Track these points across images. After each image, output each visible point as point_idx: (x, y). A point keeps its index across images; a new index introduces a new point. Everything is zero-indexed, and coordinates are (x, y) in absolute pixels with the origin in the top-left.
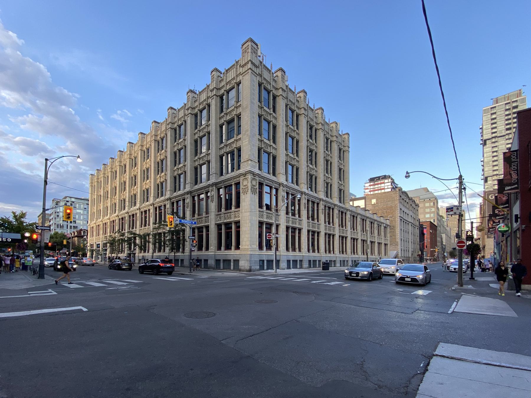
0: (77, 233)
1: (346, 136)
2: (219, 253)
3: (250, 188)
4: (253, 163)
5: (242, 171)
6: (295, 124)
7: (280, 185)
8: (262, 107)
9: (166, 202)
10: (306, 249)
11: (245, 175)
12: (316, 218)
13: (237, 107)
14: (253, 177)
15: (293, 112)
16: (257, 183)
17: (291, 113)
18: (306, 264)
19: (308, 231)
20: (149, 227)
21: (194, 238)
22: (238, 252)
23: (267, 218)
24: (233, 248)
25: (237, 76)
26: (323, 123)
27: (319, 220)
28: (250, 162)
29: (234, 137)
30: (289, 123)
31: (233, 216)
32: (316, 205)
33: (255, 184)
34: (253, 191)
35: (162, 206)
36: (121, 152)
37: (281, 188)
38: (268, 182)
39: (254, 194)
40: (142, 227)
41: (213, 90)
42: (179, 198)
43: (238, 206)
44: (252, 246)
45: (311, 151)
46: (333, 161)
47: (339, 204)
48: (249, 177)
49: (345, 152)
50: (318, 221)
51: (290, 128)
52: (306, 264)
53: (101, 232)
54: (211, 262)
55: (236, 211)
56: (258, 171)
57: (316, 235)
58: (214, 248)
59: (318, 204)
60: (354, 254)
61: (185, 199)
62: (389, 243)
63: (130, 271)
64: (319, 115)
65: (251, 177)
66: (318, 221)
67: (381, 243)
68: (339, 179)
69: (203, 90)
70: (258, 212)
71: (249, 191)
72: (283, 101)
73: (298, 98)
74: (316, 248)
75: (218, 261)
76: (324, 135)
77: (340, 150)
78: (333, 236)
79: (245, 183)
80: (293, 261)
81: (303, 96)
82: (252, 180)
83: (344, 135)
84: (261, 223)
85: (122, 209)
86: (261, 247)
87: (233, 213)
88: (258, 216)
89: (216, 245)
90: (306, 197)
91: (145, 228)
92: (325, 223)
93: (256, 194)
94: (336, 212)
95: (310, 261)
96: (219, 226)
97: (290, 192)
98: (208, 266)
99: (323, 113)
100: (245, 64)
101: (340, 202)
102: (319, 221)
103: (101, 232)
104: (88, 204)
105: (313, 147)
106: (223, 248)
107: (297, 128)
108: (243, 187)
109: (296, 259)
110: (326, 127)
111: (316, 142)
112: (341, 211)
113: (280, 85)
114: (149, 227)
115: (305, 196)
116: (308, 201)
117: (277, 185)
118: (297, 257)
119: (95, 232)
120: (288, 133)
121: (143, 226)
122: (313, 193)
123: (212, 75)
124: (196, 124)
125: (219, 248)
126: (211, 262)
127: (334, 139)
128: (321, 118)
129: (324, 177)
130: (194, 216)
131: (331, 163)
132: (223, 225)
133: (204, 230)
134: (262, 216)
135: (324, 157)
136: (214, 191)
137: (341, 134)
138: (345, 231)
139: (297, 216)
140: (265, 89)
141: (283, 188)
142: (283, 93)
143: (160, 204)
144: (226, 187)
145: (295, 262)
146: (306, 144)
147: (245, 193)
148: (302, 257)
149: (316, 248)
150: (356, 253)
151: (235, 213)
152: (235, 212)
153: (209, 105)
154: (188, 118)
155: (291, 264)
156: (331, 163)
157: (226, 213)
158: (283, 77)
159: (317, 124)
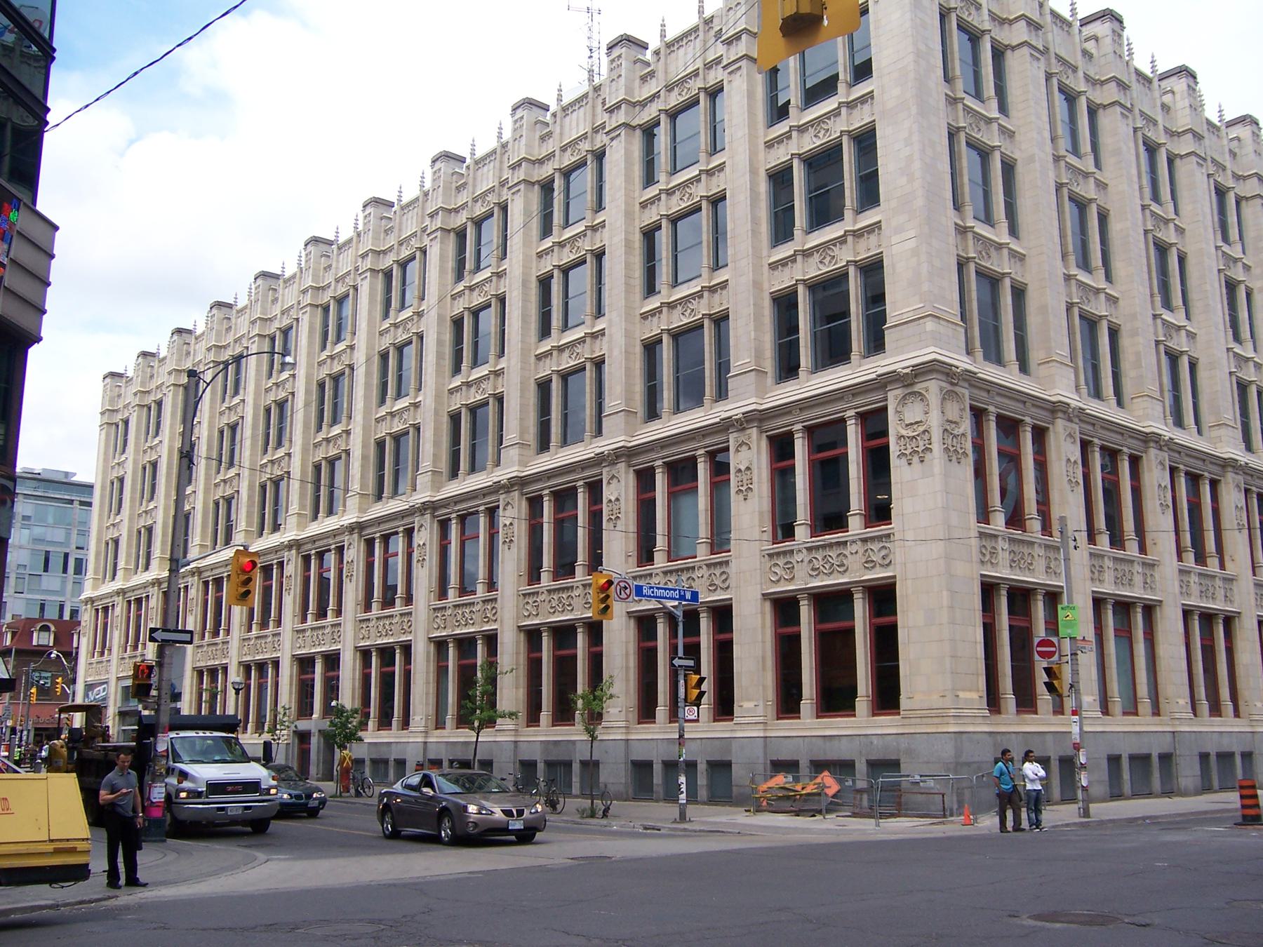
0: (14, 634)
1: (1180, 85)
2: (787, 728)
3: (936, 435)
4: (942, 328)
5: (895, 359)
6: (1086, 146)
7: (1224, 467)
8: (955, 99)
9: (116, 598)
10: (1184, 701)
11: (909, 380)
12: (1189, 544)
13: (594, 228)
14: (950, 387)
15: (974, 37)
16: (962, 410)
17: (969, 45)
18: (1188, 773)
19: (1187, 613)
20: (406, 609)
21: (691, 663)
22: (886, 725)
23: (1118, 581)
24: (862, 703)
25: (708, 66)
26: (1035, 16)
27: (1227, 558)
28: (930, 325)
29: (839, 216)
30: (1064, 144)
31: (578, 603)
32: (1125, 468)
33: (956, 419)
34: (952, 454)
35: (477, 512)
36: (271, 282)
37: (1153, 452)
38: (1007, 401)
39: (954, 458)
40: (250, 629)
41: (617, 106)
42: (139, 592)
43: (880, 512)
44: (962, 694)
45: (1081, 205)
46: (1190, 249)
47: (1166, 430)
48: (932, 387)
49: (1243, 203)
50: (1143, 549)
51: (1069, 166)
52: (1188, 773)
53: (116, 638)
54: (614, 775)
55: (872, 539)
56: (965, 359)
57: (1139, 618)
58: (760, 711)
59: (1135, 461)
60: (1216, 710)
61: (413, 528)
62: (1244, 602)
63: (312, 821)
64: (1178, 96)
65: (941, 389)
66: (1143, 549)
67: (1229, 621)
68: (1158, 299)
69: (686, 35)
70: (975, 542)
71: (937, 447)
72: (1035, 64)
73: (1087, 40)
74: (1225, 693)
75: (642, 768)
76: (1135, 130)
77: (1221, 192)
78: (1229, 621)
79: (913, 412)
80: (1132, 758)
81: (1109, 32)
82: (944, 399)
83: (1086, 22)
84: (989, 589)
85: (263, 529)
86: (993, 701)
87: (854, 548)
88: (976, 555)
89: (771, 693)
90: (1240, 478)
91: (387, 612)
92: (1180, 559)
93: (963, 461)
94: (1155, 476)
95: (1114, 760)
96: (785, 608)
97: (1096, 441)
98: (734, 789)
99: (1120, 36)
100: (737, 37)
101: (1179, 422)
102: (1228, 564)
103: (116, 638)
104: (90, 504)
105: (1088, 190)
106: (545, 716)
107: (1003, 108)
108: (904, 432)
109: (1144, 751)
110: (1209, 140)
111: (1176, 213)
112: (1000, 418)
113: (1183, 120)
114: (406, 609)
115: (1236, 477)
116: (1085, 446)
117: (1135, 442)
118: (384, 749)
119: (116, 634)
120: (1062, 184)
121: (207, 634)
122: (1105, 410)
123: (516, 118)
124: (461, 263)
125: (788, 703)
126: (614, 775)
127: (1184, 146)
128: (1188, 111)
129: (1155, 326)
130: (443, 594)
131: (1249, 295)
132: (270, 666)
133: (581, 640)
134: (987, 556)
135: (1146, 232)
136: (754, 446)
137: (1215, 120)
138: (1218, 583)
139: (1035, 525)
140: (1063, 90)
141: (1069, 424)
142: (1034, 33)
143: (465, 505)
144: (863, 417)
145: (1141, 761)
146: (1140, 222)
147: (920, 454)
148: (1169, 738)
149: (1225, 693)
150: (1228, 706)
151: (712, 571)
152: (864, 541)
153: (504, 208)
154: (516, 197)
155: (1126, 775)
156: (1182, 260)
157: (817, 548)
158: (1116, 38)
159: (1171, 134)
